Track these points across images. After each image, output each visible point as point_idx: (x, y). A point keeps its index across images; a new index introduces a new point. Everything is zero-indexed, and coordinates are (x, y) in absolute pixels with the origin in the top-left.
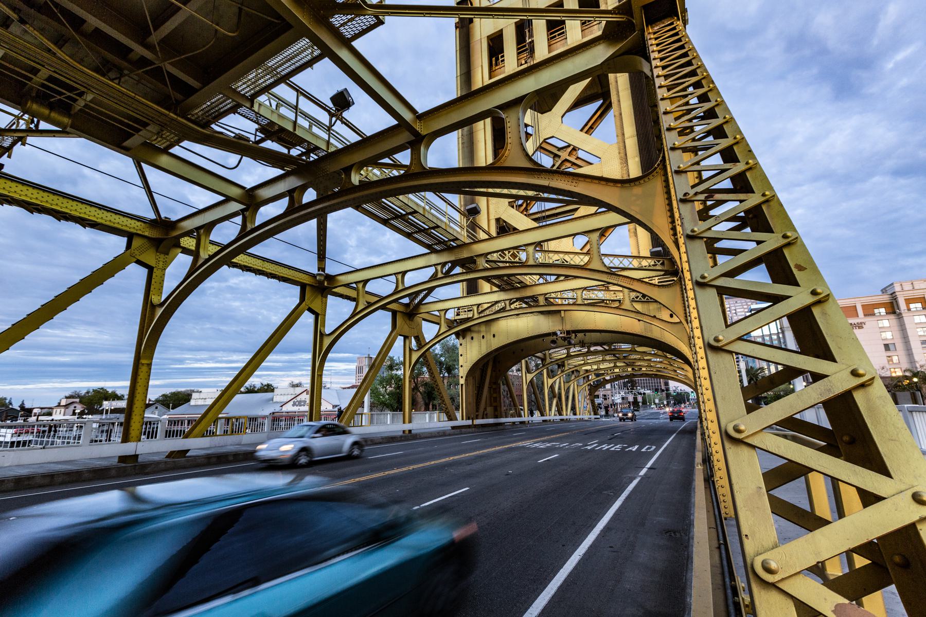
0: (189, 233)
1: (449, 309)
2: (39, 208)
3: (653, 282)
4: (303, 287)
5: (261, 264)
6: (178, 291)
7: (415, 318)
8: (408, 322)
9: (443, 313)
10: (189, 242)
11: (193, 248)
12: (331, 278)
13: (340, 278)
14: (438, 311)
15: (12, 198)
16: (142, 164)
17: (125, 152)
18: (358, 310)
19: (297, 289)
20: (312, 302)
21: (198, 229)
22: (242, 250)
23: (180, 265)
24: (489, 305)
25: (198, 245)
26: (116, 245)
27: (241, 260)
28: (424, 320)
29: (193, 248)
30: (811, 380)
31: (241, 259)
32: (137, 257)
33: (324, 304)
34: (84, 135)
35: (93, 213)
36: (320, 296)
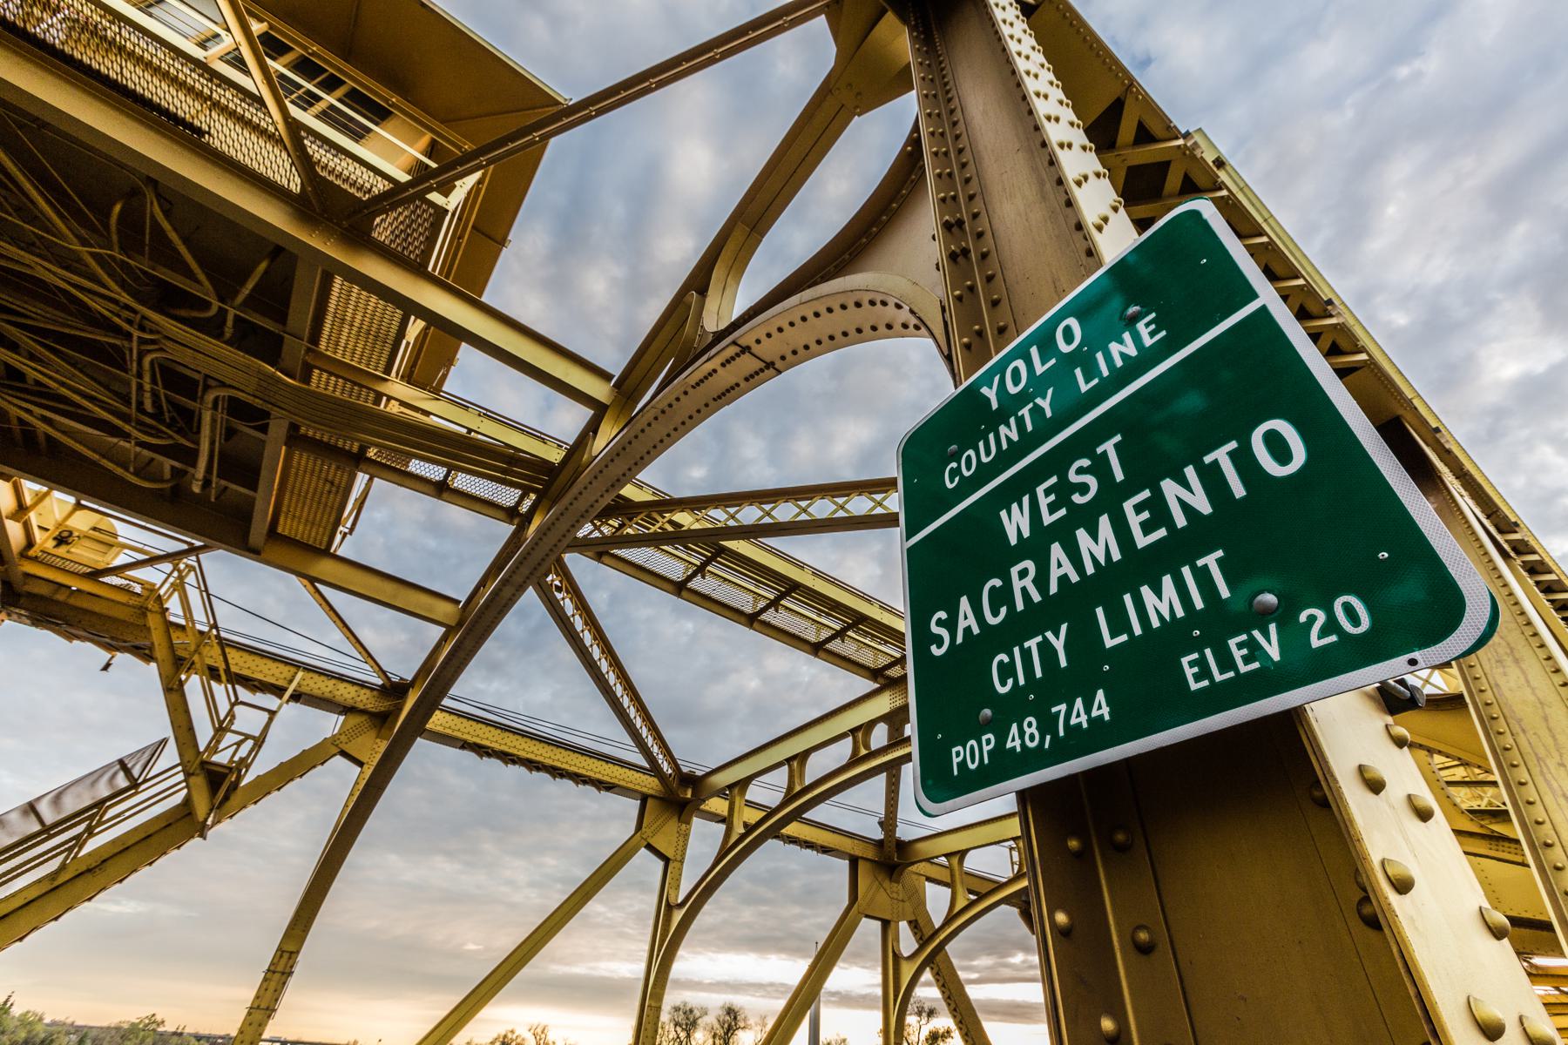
0: (720, 793)
1: (967, 851)
2: (515, 758)
3: (1444, 759)
4: (854, 862)
5: (499, 738)
6: (704, 884)
7: (905, 874)
8: (887, 884)
9: (955, 860)
10: (718, 805)
11: (725, 813)
12: (903, 847)
13: (920, 846)
14: (946, 855)
15: (567, 771)
16: (316, 584)
17: (254, 556)
18: (958, 907)
19: (633, 806)
20: (654, 834)
21: (731, 787)
22: (796, 815)
23: (703, 839)
24: (141, 557)
25: (731, 809)
26: (329, 724)
27: (639, 784)
28: (929, 879)
29: (725, 813)
30: (385, 398)
31: (792, 829)
32: (340, 745)
33: (681, 839)
34: (223, 546)
35: (320, 684)
36: (675, 819)
